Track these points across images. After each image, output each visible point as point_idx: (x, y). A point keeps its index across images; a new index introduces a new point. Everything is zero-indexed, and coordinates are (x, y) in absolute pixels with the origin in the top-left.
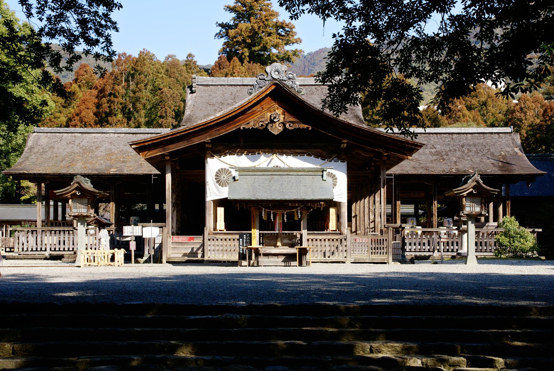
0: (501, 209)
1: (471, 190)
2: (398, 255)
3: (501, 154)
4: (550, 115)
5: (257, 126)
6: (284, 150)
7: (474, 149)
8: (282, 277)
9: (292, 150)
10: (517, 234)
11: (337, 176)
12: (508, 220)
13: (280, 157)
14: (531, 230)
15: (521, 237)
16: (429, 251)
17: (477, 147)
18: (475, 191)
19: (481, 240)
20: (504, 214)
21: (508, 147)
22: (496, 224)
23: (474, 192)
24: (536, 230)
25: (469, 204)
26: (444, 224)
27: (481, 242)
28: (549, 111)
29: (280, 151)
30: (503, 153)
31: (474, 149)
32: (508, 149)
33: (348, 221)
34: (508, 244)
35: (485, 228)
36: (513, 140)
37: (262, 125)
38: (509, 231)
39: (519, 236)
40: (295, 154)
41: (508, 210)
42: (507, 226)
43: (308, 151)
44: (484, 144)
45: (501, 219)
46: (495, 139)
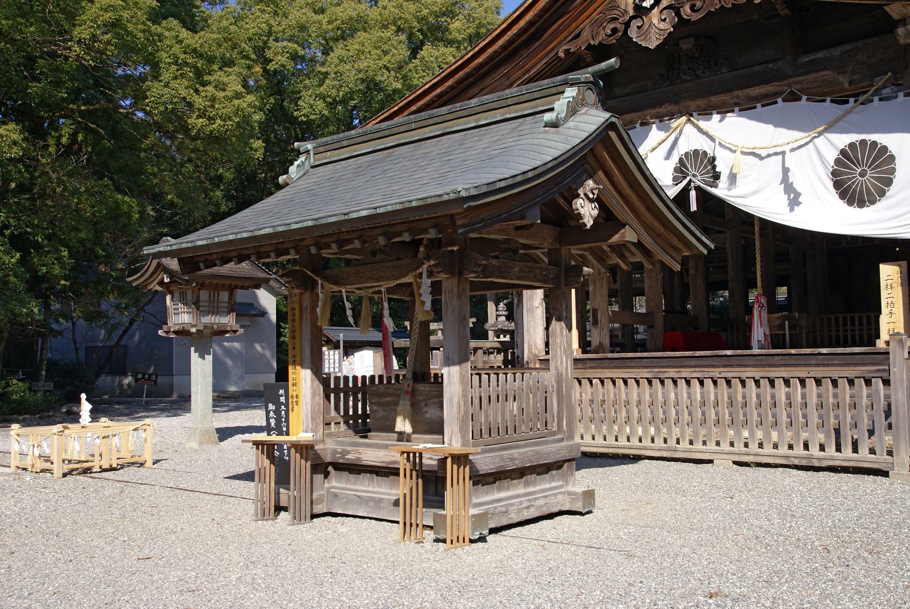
5: (601, 37)
6: (714, 99)
8: (854, 468)
9: (736, 93)
11: (893, 149)
13: (702, 124)
29: (701, 102)
37: (615, 31)
40: (745, 107)
43: (789, 85)
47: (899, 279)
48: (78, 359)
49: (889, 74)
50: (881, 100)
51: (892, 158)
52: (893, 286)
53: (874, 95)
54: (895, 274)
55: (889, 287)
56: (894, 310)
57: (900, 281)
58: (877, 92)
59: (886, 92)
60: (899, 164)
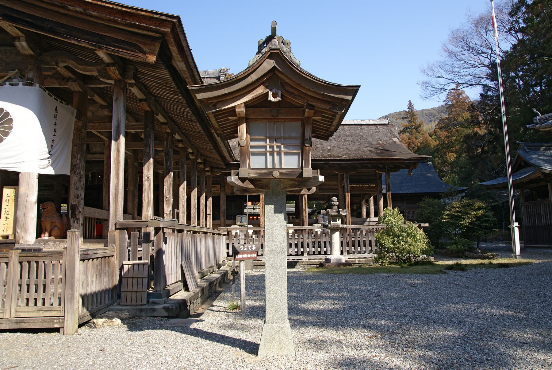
0: (381, 203)
1: (261, 90)
2: (139, 294)
3: (379, 143)
4: (412, 146)
7: (351, 139)
10: (403, 231)
11: (12, 115)
12: (391, 213)
14: (417, 225)
15: (408, 235)
16: (297, 254)
17: (354, 137)
18: (274, 96)
19: (359, 239)
20: (385, 206)
21: (386, 136)
22: (376, 219)
23: (271, 98)
24: (423, 225)
25: (262, 143)
26: (319, 220)
27: (359, 242)
28: (411, 143)
30: (381, 142)
31: (351, 139)
32: (386, 139)
33: (198, 220)
34: (391, 245)
35: (366, 224)
36: (391, 130)
38: (392, 227)
39: (405, 234)
41: (390, 202)
42: (389, 220)
44: (361, 134)
45: (382, 212)
46: (372, 130)
47: (14, 197)
48: (504, 52)
49: (17, 70)
50: (10, 84)
51: (11, 120)
52: (10, 201)
53: (6, 81)
54: (12, 194)
55: (7, 201)
56: (9, 216)
57: (14, 198)
58: (10, 79)
59: (15, 81)
60: (15, 124)
